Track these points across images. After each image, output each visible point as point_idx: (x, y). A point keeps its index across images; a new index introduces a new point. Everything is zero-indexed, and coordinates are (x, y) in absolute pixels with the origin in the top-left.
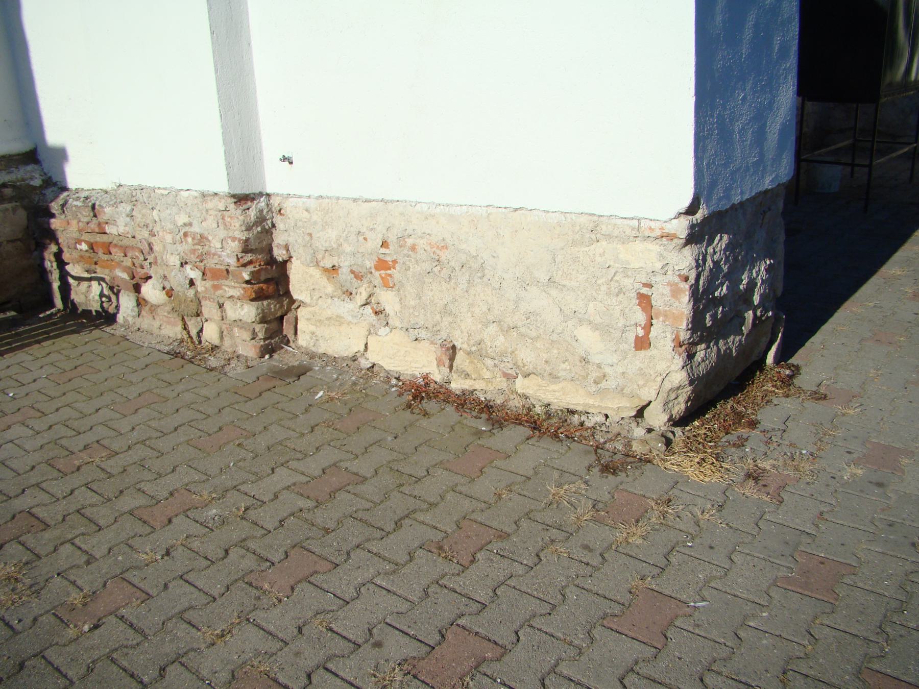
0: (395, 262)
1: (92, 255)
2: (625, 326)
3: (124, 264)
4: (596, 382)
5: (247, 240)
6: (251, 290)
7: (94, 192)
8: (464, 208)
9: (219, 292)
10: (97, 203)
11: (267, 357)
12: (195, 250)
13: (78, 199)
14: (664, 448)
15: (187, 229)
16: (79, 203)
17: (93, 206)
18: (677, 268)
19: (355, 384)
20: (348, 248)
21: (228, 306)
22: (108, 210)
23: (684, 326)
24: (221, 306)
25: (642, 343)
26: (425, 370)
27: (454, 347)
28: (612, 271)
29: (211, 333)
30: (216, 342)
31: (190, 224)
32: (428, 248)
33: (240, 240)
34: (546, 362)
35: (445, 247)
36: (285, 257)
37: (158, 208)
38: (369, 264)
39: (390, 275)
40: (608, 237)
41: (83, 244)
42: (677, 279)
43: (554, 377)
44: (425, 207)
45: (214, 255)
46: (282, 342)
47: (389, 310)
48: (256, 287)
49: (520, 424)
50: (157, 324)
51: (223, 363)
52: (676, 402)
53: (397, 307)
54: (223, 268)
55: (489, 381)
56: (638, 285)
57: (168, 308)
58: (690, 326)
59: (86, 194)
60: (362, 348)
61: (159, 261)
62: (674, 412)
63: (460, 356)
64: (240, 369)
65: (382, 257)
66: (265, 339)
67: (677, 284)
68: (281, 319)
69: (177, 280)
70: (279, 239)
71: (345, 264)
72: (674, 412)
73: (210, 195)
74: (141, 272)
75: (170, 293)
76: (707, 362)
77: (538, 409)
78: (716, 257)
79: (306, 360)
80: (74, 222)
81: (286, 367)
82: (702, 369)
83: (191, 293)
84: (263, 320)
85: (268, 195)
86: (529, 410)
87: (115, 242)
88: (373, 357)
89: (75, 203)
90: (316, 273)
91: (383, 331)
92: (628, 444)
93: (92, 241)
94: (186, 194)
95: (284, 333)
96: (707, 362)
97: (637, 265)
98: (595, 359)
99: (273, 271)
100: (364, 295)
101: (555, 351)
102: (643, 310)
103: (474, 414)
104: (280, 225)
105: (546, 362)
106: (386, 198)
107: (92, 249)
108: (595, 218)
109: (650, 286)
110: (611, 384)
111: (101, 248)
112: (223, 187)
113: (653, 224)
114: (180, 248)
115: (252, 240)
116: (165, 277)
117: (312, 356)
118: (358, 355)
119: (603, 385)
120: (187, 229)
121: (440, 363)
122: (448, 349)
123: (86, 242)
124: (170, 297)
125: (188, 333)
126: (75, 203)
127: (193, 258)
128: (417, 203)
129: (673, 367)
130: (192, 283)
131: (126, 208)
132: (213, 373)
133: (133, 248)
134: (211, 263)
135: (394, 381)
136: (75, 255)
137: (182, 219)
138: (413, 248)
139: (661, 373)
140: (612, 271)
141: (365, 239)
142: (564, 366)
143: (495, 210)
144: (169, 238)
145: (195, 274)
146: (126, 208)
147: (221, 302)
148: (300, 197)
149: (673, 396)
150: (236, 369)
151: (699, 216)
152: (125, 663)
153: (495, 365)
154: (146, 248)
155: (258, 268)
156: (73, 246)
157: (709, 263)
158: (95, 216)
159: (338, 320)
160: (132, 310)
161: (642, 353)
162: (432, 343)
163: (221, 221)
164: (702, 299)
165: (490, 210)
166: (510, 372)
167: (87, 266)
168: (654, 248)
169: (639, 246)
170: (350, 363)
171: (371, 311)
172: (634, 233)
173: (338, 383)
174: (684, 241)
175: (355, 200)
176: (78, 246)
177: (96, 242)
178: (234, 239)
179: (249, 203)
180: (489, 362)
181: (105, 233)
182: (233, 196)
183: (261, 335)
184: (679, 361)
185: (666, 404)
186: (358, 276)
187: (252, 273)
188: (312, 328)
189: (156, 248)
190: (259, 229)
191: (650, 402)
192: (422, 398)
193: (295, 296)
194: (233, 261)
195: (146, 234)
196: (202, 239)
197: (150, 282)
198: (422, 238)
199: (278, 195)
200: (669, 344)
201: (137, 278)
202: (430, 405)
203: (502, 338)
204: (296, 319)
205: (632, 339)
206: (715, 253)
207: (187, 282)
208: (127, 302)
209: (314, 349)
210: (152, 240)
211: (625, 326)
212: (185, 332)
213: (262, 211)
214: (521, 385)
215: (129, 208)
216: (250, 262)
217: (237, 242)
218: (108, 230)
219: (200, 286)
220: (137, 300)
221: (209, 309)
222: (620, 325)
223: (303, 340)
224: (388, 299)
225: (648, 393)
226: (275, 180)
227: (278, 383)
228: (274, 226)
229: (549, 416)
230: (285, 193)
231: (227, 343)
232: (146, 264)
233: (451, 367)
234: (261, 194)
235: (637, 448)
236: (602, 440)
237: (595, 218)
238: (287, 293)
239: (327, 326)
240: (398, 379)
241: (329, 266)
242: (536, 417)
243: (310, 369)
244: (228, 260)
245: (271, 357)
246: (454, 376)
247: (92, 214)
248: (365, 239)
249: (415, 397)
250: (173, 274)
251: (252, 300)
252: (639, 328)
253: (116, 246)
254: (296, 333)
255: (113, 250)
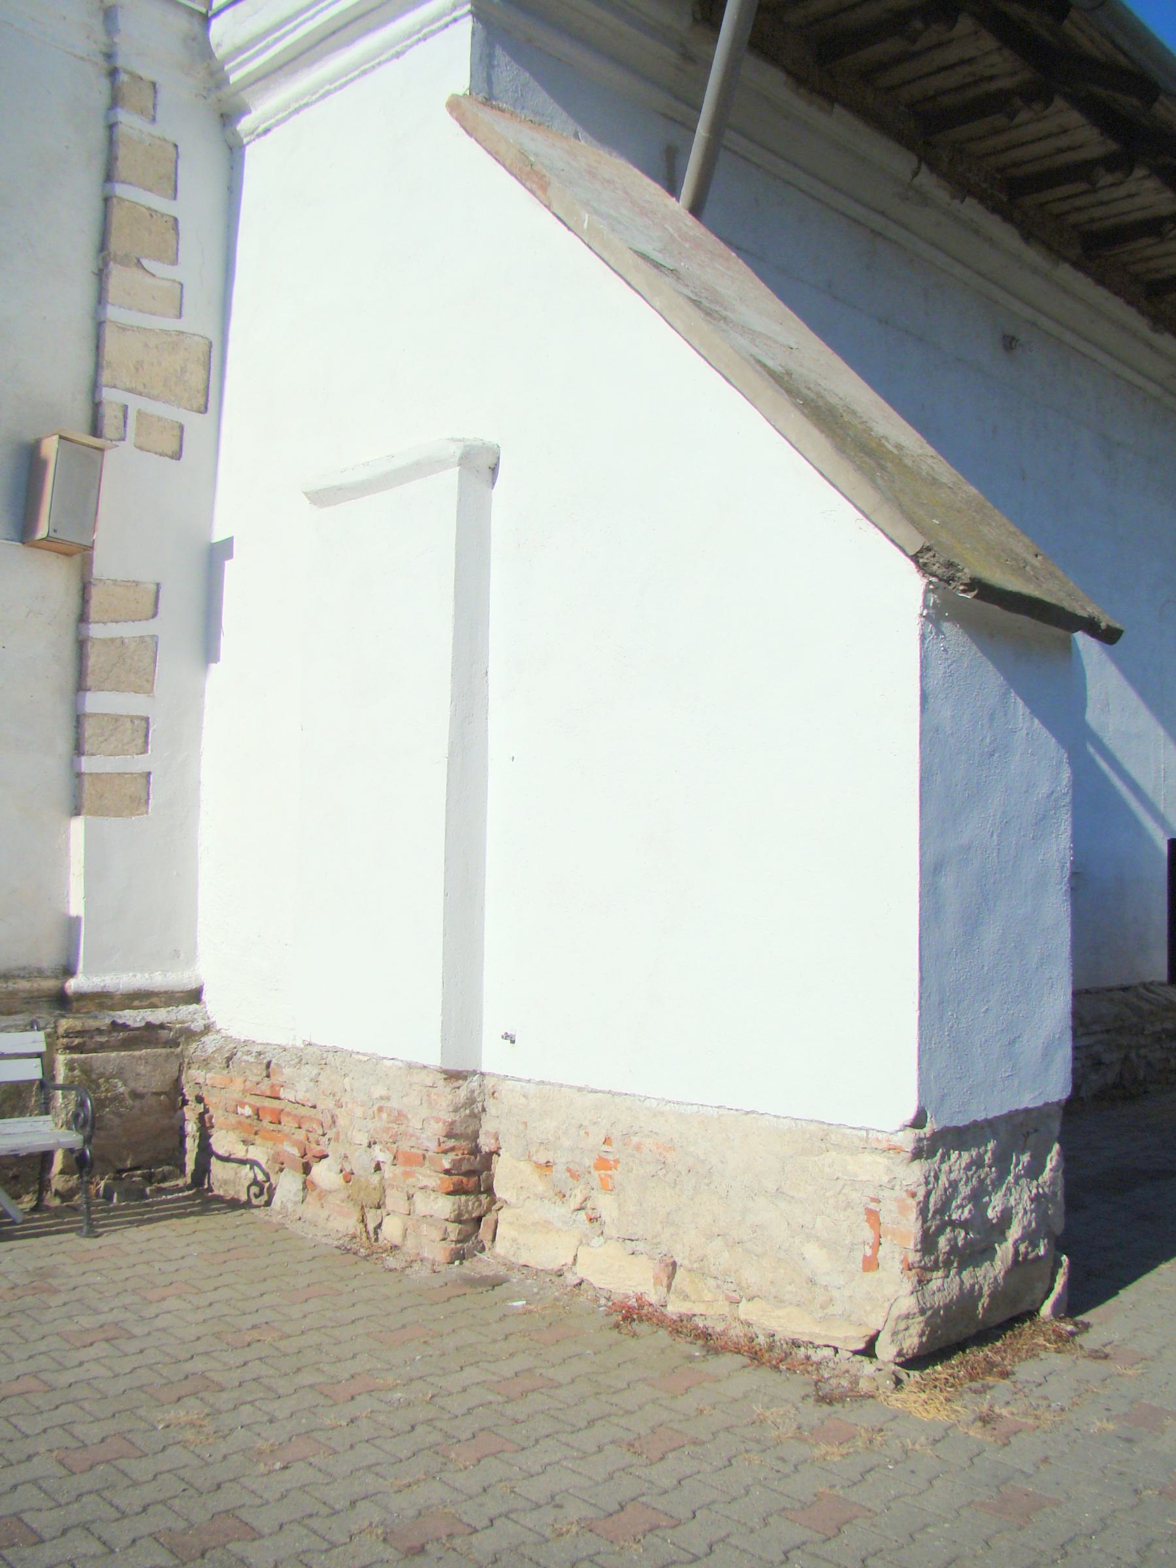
0: (617, 1161)
1: (255, 1122)
2: (853, 1244)
3: (295, 1137)
4: (822, 1307)
5: (453, 1123)
6: (449, 1182)
7: (269, 1048)
8: (695, 1107)
9: (411, 1181)
10: (274, 1061)
11: (457, 1262)
12: (389, 1129)
13: (249, 1053)
14: (893, 1386)
15: (383, 1103)
16: (250, 1059)
17: (268, 1065)
18: (904, 1183)
19: (556, 1299)
20: (566, 1142)
21: (419, 1197)
22: (287, 1071)
23: (911, 1246)
24: (410, 1197)
25: (870, 1264)
26: (640, 1289)
27: (674, 1264)
28: (841, 1183)
29: (392, 1230)
30: (397, 1240)
31: (388, 1098)
32: (654, 1148)
33: (445, 1122)
34: (772, 1282)
35: (672, 1149)
36: (493, 1148)
37: (351, 1076)
38: (588, 1162)
39: (610, 1176)
40: (837, 1146)
41: (247, 1107)
42: (904, 1195)
43: (779, 1301)
44: (654, 1103)
45: (411, 1136)
46: (475, 1248)
47: (605, 1217)
48: (455, 1178)
49: (739, 1353)
50: (324, 1213)
51: (404, 1264)
52: (907, 1333)
53: (615, 1214)
54: (420, 1152)
55: (709, 1303)
56: (865, 1200)
57: (343, 1195)
58: (919, 1247)
59: (259, 1048)
60: (570, 1260)
61: (342, 1138)
62: (906, 1345)
63: (680, 1272)
64: (425, 1272)
65: (603, 1155)
66: (458, 1242)
67: (903, 1200)
68: (479, 1220)
69: (361, 1162)
70: (488, 1125)
71: (561, 1160)
72: (906, 1345)
73: (416, 1068)
74: (315, 1149)
75: (348, 1177)
76: (946, 1293)
77: (762, 1340)
78: (953, 1176)
79: (502, 1271)
80: (239, 1080)
81: (478, 1276)
82: (939, 1300)
83: (375, 1179)
84: (458, 1220)
85: (482, 1074)
86: (752, 1340)
87: (287, 1109)
88: (581, 1272)
89: (246, 1058)
90: (526, 1167)
91: (597, 1241)
92: (855, 1381)
93: (258, 1105)
94: (389, 1063)
95: (480, 1237)
96: (946, 1293)
97: (865, 1179)
98: (822, 1280)
99: (476, 1162)
100: (579, 1199)
101: (782, 1271)
102: (872, 1226)
103: (689, 1339)
104: (492, 1110)
105: (772, 1282)
106: (614, 1090)
107: (258, 1114)
108: (825, 1127)
109: (878, 1201)
110: (836, 1309)
111: (265, 1117)
112: (434, 1058)
113: (880, 1135)
114: (370, 1125)
115: (458, 1124)
116: (346, 1157)
117: (510, 1267)
118: (565, 1268)
119: (830, 1310)
120: (383, 1103)
121: (657, 1281)
122: (667, 1265)
123: (251, 1106)
124: (348, 1182)
125: (366, 1226)
126: (246, 1058)
127: (386, 1137)
128: (647, 1098)
129: (901, 1292)
130: (378, 1168)
131: (310, 1071)
132: (393, 1274)
133: (311, 1119)
134: (404, 1146)
135: (603, 1301)
136: (233, 1119)
137: (379, 1091)
138: (638, 1147)
139: (886, 1300)
140: (841, 1183)
141: (587, 1133)
142: (789, 1288)
143: (726, 1112)
144: (359, 1112)
145: (380, 1154)
146: (310, 1071)
147: (411, 1192)
148: (519, 1080)
149: (902, 1325)
150: (420, 1272)
151: (927, 1130)
152: (317, 1494)
153: (718, 1287)
154: (327, 1121)
155: (460, 1156)
156: (232, 1109)
157: (943, 1180)
158: (268, 1076)
159: (546, 1226)
160: (295, 1194)
161: (871, 1274)
162: (651, 1258)
163: (425, 1098)
164: (933, 1219)
165: (721, 1111)
166: (734, 1294)
167: (245, 1136)
168: (882, 1160)
169: (868, 1158)
170: (554, 1278)
171: (584, 1217)
172: (862, 1144)
173: (538, 1297)
174: (909, 1155)
175: (580, 1089)
176: (240, 1110)
177: (264, 1108)
178: (438, 1120)
179: (461, 1082)
180: (711, 1282)
181: (279, 1098)
182: (445, 1072)
183: (453, 1236)
184: (908, 1286)
185: (895, 1333)
186: (574, 1175)
187: (454, 1162)
188: (514, 1234)
189: (341, 1121)
190: (468, 1112)
191: (879, 1332)
192: (634, 1320)
193: (499, 1193)
194: (433, 1146)
195: (330, 1103)
196: (399, 1118)
197: (324, 1161)
198: (649, 1136)
199: (493, 1075)
200: (898, 1267)
201: (309, 1156)
202: (642, 1328)
203: (726, 1254)
204: (497, 1222)
205: (860, 1259)
206: (950, 1171)
207: (373, 1165)
208: (287, 1185)
209: (513, 1260)
210: (337, 1111)
211: (853, 1244)
212: (361, 1225)
213: (473, 1091)
214: (745, 1310)
215: (315, 1071)
216: (453, 1149)
217: (441, 1124)
218: (282, 1094)
219: (388, 1170)
220: (304, 1183)
221: (395, 1200)
222: (847, 1242)
223: (502, 1247)
224: (605, 1204)
225: (875, 1321)
226: (493, 1058)
227: (468, 1290)
228: (484, 1110)
229: (771, 1347)
230: (503, 1073)
231: (410, 1243)
232: (324, 1140)
233: (669, 1286)
234: (474, 1073)
235: (864, 1386)
236: (826, 1376)
237: (825, 1127)
238: (490, 1190)
239: (532, 1232)
240: (608, 1299)
241: (543, 1161)
242: (758, 1348)
243: (508, 1281)
244: (427, 1144)
245: (461, 1263)
246: (672, 1297)
247: (265, 1073)
248: (587, 1133)
249: (625, 1318)
250: (357, 1154)
251: (449, 1193)
252: (867, 1247)
253: (289, 1114)
254: (494, 1239)
255: (284, 1119)
